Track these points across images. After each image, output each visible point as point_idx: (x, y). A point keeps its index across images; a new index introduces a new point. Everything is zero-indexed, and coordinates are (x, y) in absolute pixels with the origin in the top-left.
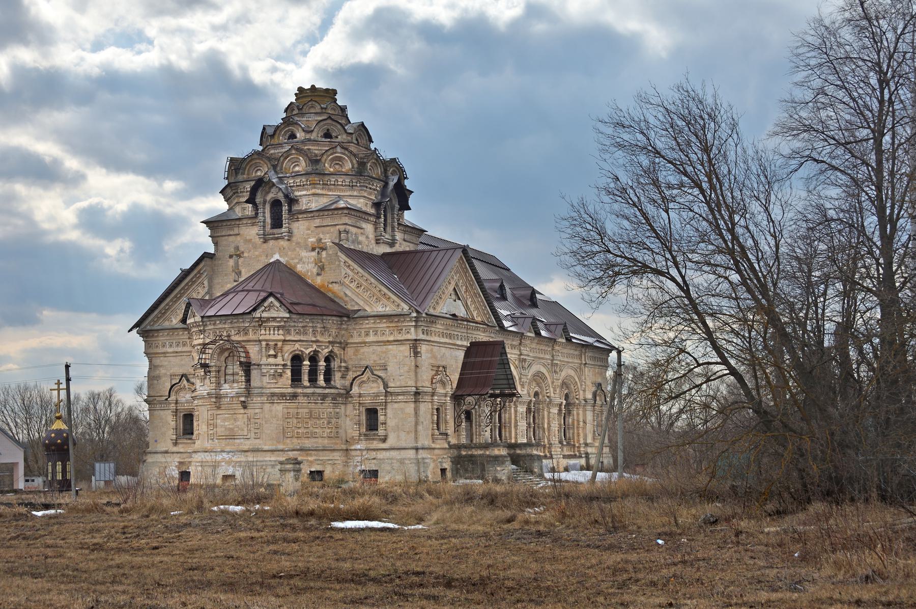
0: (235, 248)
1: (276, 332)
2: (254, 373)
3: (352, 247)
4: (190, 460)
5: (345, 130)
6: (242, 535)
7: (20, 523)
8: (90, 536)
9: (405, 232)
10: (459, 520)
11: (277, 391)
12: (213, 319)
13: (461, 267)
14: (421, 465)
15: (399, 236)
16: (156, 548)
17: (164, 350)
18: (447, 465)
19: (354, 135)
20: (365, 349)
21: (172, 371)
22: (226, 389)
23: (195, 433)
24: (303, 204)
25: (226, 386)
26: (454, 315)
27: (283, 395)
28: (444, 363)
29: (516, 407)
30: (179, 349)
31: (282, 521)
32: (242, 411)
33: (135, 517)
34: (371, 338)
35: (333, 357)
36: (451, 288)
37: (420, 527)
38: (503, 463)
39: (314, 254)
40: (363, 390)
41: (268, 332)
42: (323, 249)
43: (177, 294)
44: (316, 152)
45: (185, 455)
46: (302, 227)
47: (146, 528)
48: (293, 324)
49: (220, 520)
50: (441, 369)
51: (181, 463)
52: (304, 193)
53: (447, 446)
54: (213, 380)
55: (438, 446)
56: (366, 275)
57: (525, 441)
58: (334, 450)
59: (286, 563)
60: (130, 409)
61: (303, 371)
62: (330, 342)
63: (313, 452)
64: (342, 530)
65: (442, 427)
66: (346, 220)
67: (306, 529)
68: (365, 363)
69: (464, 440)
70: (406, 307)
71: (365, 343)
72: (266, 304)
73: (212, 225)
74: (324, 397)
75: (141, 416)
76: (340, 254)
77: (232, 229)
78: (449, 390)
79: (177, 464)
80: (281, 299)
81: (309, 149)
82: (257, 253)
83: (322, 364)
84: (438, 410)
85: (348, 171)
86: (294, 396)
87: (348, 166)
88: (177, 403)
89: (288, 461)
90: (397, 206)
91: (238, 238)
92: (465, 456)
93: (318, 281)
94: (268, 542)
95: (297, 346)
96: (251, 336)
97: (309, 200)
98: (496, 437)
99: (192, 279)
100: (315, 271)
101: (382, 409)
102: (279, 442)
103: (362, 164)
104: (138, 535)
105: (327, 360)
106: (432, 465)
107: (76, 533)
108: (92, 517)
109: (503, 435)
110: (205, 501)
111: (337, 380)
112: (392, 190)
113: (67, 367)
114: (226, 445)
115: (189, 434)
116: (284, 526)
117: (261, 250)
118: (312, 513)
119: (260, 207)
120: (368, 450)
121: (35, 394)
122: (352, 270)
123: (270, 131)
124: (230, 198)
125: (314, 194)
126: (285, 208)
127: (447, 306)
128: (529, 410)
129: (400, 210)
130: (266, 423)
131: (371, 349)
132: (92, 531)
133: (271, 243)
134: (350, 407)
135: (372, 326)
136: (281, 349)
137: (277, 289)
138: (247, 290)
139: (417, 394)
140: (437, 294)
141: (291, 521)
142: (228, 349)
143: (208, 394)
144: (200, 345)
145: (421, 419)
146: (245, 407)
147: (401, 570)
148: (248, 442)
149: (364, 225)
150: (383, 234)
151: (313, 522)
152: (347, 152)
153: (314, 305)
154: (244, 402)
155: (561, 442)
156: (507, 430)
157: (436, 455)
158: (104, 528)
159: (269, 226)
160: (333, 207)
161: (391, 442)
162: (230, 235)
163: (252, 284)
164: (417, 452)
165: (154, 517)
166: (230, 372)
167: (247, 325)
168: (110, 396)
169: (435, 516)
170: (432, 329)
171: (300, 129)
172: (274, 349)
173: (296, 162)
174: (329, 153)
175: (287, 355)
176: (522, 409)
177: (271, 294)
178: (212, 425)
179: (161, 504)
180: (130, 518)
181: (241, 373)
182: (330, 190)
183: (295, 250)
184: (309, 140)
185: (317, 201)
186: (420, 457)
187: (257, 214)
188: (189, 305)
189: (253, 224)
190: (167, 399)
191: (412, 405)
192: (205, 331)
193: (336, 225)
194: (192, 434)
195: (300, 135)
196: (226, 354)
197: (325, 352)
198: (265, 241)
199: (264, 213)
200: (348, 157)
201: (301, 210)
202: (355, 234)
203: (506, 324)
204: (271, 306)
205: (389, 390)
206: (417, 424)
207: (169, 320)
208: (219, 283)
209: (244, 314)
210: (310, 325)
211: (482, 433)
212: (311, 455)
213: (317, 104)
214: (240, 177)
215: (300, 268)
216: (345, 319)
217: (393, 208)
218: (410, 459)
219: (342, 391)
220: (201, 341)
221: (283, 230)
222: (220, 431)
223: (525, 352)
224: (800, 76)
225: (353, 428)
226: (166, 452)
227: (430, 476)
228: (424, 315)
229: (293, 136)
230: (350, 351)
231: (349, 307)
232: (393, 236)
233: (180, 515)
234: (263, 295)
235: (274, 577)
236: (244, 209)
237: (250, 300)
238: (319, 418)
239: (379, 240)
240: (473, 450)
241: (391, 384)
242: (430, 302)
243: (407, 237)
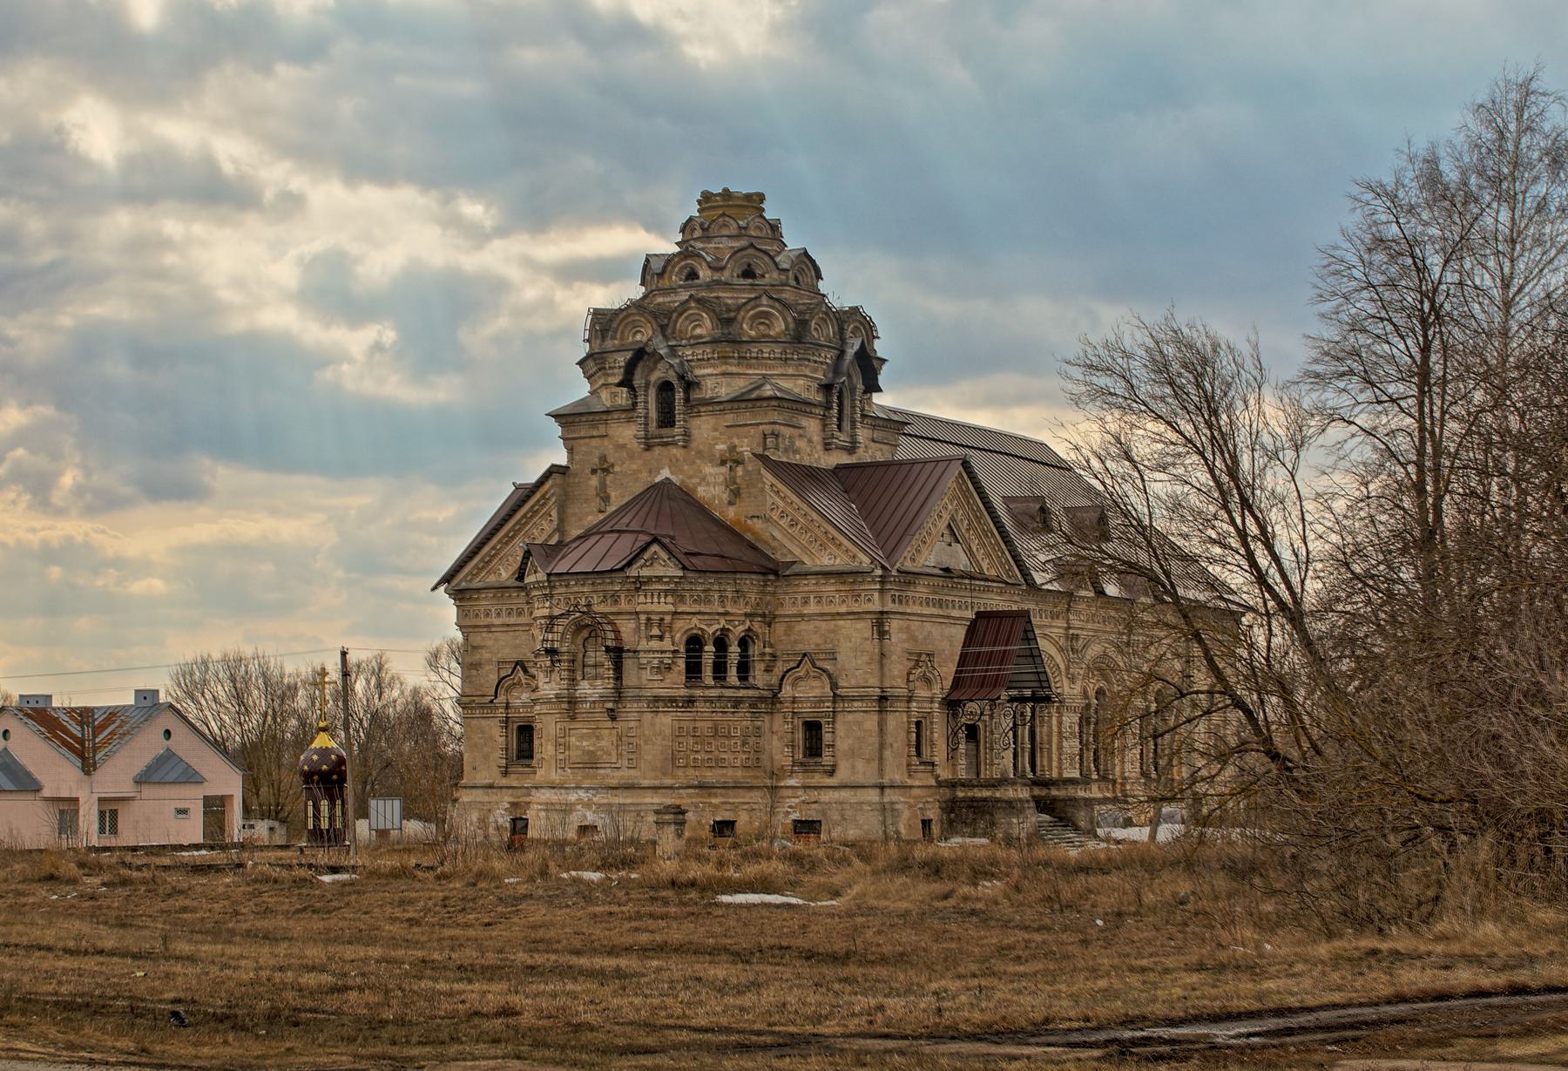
0: (600, 458)
1: (662, 600)
2: (629, 664)
3: (784, 460)
4: (527, 799)
5: (776, 265)
6: (598, 909)
7: (304, 891)
8: (401, 909)
9: (874, 427)
10: (884, 895)
11: (663, 692)
12: (565, 577)
13: (961, 490)
14: (888, 814)
15: (863, 434)
16: (489, 924)
17: (488, 621)
18: (933, 814)
19: (790, 273)
20: (803, 626)
22: (585, 689)
23: (537, 756)
25: (585, 684)
26: (947, 570)
27: (672, 701)
28: (929, 648)
29: (1060, 715)
30: (512, 620)
31: (652, 893)
32: (609, 724)
33: (458, 885)
34: (812, 608)
35: (751, 638)
36: (942, 525)
37: (834, 902)
38: (1021, 811)
39: (724, 470)
40: (800, 692)
42: (738, 462)
43: (509, 532)
44: (730, 301)
45: (519, 792)
46: (704, 427)
47: (474, 900)
48: (688, 587)
49: (570, 890)
50: (923, 657)
51: (514, 805)
52: (709, 371)
53: (933, 783)
54: (565, 674)
55: (917, 783)
56: (804, 506)
57: (1076, 774)
58: (751, 788)
59: (644, 938)
60: (415, 692)
61: (704, 661)
62: (746, 615)
63: (719, 791)
64: (729, 905)
65: (926, 751)
66: (775, 417)
67: (682, 904)
68: (801, 648)
69: (962, 774)
70: (866, 560)
71: (802, 616)
72: (647, 555)
73: (564, 420)
74: (737, 702)
75: (436, 709)
76: (763, 471)
77: (594, 427)
78: (939, 691)
79: (507, 806)
80: (671, 546)
81: (718, 298)
82: (634, 467)
83: (734, 650)
84: (918, 724)
85: (779, 334)
86: (690, 701)
87: (779, 326)
88: (507, 707)
89: (667, 809)
90: (860, 387)
91: (606, 442)
92: (963, 800)
93: (731, 514)
94: (630, 919)
95: (695, 621)
96: (624, 606)
97: (717, 383)
98: (1024, 767)
99: (533, 507)
100: (725, 497)
101: (828, 723)
102: (664, 774)
103: (802, 324)
104: (464, 909)
105: (744, 643)
106: (906, 814)
107: (381, 906)
108: (402, 884)
109: (1038, 763)
110: (552, 864)
111: (759, 676)
112: (852, 362)
113: (344, 654)
114: (584, 778)
115: (527, 757)
116: (653, 899)
117: (640, 462)
118: (693, 884)
119: (641, 392)
120: (805, 787)
121: (253, 668)
122: (783, 499)
123: (656, 266)
124: (592, 376)
125: (724, 374)
126: (679, 395)
127: (931, 553)
128: (1084, 721)
129: (865, 392)
130: (646, 742)
131: (811, 626)
132: (402, 903)
133: (657, 450)
134: (778, 719)
135: (812, 588)
136: (670, 627)
137: (664, 530)
138: (618, 531)
139: (883, 699)
140: (917, 536)
141: (664, 894)
142: (587, 626)
143: (557, 696)
144: (544, 617)
145: (889, 739)
146: (613, 719)
147: (764, 946)
148: (617, 774)
149: (804, 422)
150: (837, 434)
151: (693, 894)
152: (777, 305)
153: (722, 557)
154: (612, 710)
155: (1144, 774)
156: (1045, 754)
157: (915, 797)
158: (417, 900)
159: (655, 424)
160: (753, 396)
161: (842, 775)
163: (626, 520)
164: (882, 794)
165: (482, 885)
166: (590, 661)
167: (617, 588)
168: (380, 670)
169: (856, 889)
170: (909, 593)
171: (704, 264)
172: (660, 626)
173: (697, 320)
174: (748, 307)
175: (678, 635)
176: (1071, 720)
177: (655, 540)
178: (562, 744)
179: (493, 868)
180: (451, 886)
181: (608, 664)
182: (750, 366)
183: (694, 462)
184: (718, 282)
185: (729, 385)
186: (886, 800)
187: (635, 404)
188: (527, 555)
189: (629, 420)
190: (492, 702)
191: (875, 717)
192: (552, 596)
194: (532, 757)
195: (704, 274)
196: (585, 633)
197: (739, 630)
198: (648, 448)
199: (646, 402)
200: (778, 311)
201: (703, 399)
202: (790, 437)
203: (1039, 578)
204: (653, 559)
205: (838, 692)
206: (882, 746)
207: (495, 572)
208: (574, 514)
209: (611, 571)
210: (716, 587)
211: (996, 761)
212: (715, 795)
213: (732, 221)
214: (610, 344)
215: (702, 492)
216: (772, 577)
217: (853, 390)
218: (870, 803)
219: (765, 693)
220: (546, 612)
221: (676, 431)
223: (1076, 623)
224: (1327, 307)
225: (783, 752)
226: (491, 787)
227: (903, 831)
228: (894, 573)
229: (693, 275)
230: (779, 628)
231: (778, 557)
232: (853, 436)
233: (518, 883)
234: (645, 539)
236: (615, 395)
237: (625, 546)
238: (729, 737)
239: (829, 444)
240: (976, 790)
241: (842, 683)
242: (907, 552)
243: (877, 435)
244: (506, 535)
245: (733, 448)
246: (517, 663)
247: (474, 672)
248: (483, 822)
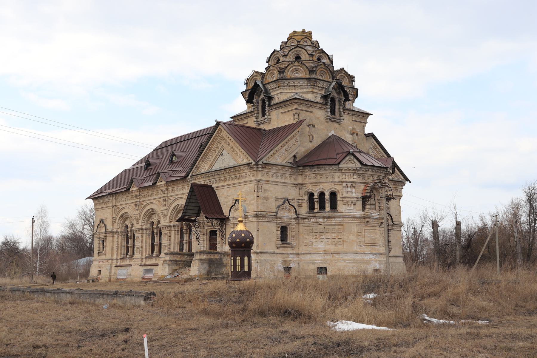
21: (276, 195)
24: (275, 101)
66: (296, 106)
82: (322, 127)
189: (321, 108)
222: (367, 240)
226: (273, 253)
245: (354, 128)
247: (265, 201)
248: (272, 269)
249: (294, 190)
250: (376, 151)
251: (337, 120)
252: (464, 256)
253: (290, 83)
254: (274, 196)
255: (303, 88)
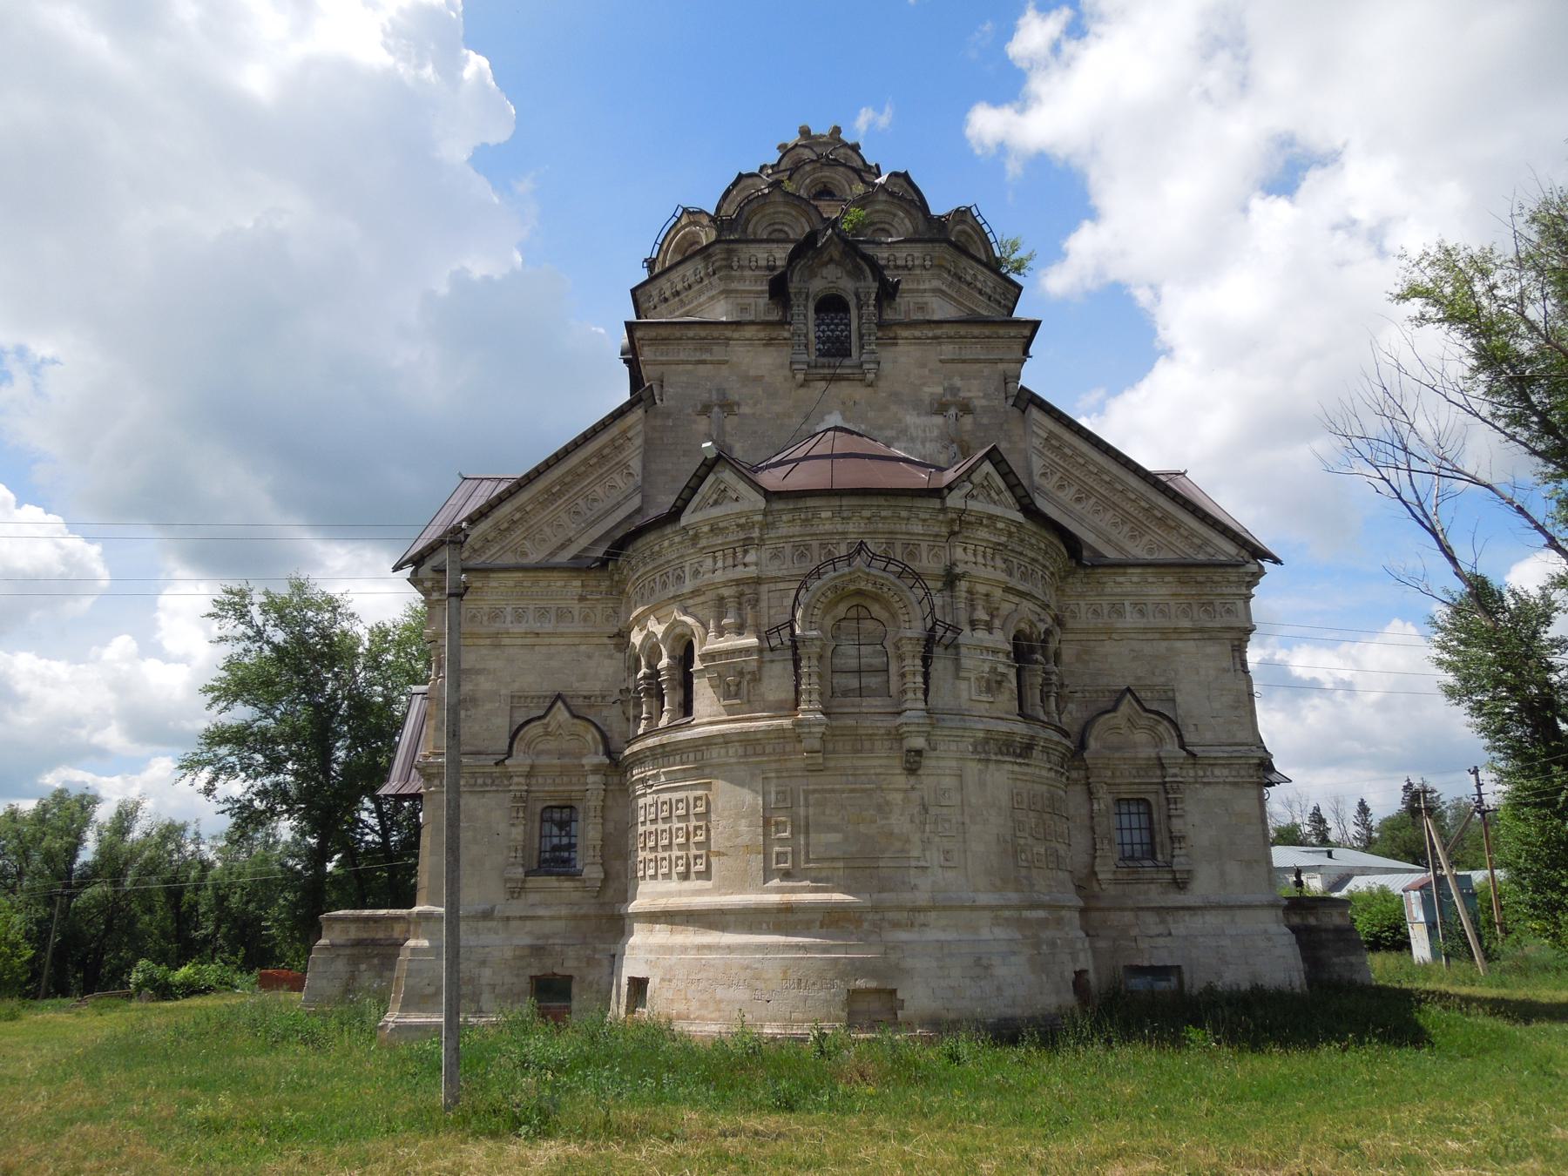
21: (516, 686)
41: (980, 560)
91: (725, 370)
146: (912, 770)
162: (703, 362)
189: (770, 342)
193: (995, 361)
235: (292, 1130)
244: (547, 490)
246: (559, 697)
249: (611, 657)
250: (1064, 456)
251: (849, 371)
252: (1527, 959)
253: (897, 255)
254: (503, 692)
255: (701, 293)
